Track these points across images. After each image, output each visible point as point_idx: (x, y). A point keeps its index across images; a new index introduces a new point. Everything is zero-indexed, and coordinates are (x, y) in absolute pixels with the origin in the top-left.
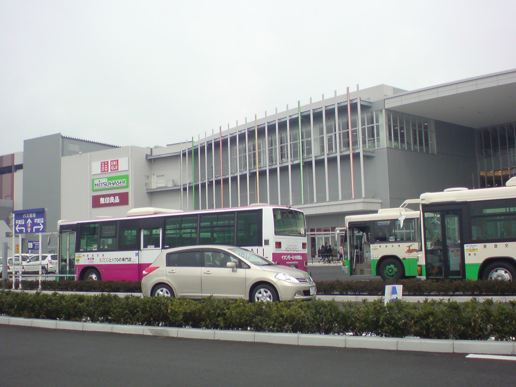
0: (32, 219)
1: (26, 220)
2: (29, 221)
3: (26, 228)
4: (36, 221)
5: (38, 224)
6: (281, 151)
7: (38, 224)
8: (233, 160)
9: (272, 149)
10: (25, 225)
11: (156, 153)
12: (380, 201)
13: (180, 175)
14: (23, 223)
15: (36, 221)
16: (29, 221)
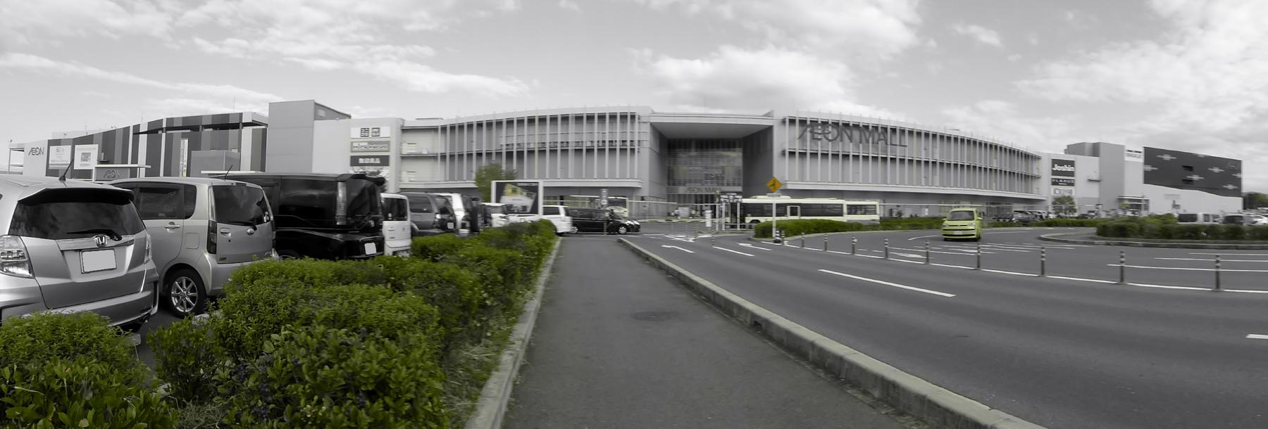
11: (407, 125)
13: (436, 145)
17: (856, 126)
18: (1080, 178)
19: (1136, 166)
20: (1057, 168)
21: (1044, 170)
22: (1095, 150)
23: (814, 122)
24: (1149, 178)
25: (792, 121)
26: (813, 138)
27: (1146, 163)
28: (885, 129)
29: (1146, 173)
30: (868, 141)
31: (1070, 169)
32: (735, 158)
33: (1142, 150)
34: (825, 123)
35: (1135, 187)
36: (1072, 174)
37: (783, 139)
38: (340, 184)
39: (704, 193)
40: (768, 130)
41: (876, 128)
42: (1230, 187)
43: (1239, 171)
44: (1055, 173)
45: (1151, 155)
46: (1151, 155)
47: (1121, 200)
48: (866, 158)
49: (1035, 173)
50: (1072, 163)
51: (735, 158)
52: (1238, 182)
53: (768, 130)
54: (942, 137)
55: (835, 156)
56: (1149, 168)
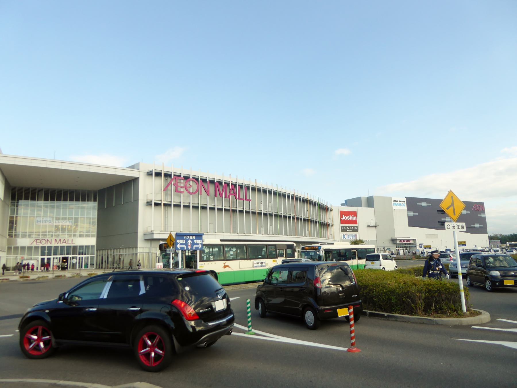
0: (192, 240)
1: (187, 240)
2: (190, 241)
3: (187, 246)
4: (195, 241)
5: (198, 244)
6: (423, 323)
7: (198, 244)
8: (97, 260)
9: (232, 210)
10: (186, 244)
12: (326, 270)
14: (184, 242)
15: (195, 241)
16: (190, 241)
17: (212, 182)
18: (361, 225)
19: (402, 212)
20: (344, 218)
21: (334, 218)
22: (370, 202)
23: (177, 176)
24: (413, 222)
25: (158, 174)
26: (176, 191)
27: (409, 210)
28: (234, 185)
29: (409, 218)
30: (221, 196)
31: (353, 218)
32: (87, 212)
33: (405, 200)
34: (186, 178)
35: (403, 230)
36: (355, 222)
37: (148, 189)
38: (141, 277)
39: (53, 244)
40: (135, 181)
41: (227, 184)
42: (477, 225)
43: (483, 211)
44: (343, 222)
45: (412, 203)
46: (412, 203)
47: (393, 241)
48: (220, 210)
49: (329, 221)
50: (354, 214)
51: (87, 212)
52: (483, 221)
53: (135, 181)
54: (275, 193)
55: (196, 207)
56: (411, 214)
